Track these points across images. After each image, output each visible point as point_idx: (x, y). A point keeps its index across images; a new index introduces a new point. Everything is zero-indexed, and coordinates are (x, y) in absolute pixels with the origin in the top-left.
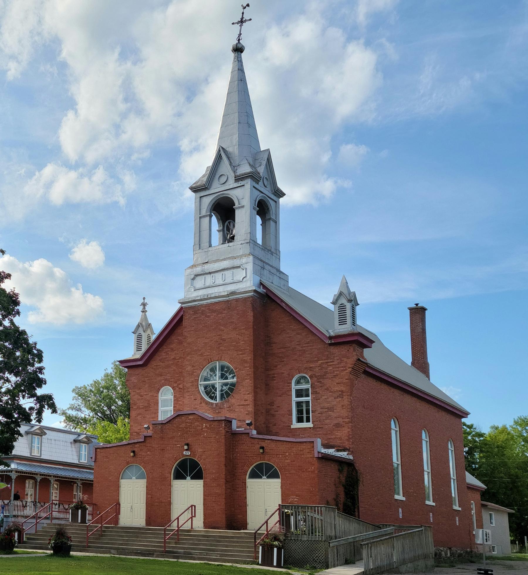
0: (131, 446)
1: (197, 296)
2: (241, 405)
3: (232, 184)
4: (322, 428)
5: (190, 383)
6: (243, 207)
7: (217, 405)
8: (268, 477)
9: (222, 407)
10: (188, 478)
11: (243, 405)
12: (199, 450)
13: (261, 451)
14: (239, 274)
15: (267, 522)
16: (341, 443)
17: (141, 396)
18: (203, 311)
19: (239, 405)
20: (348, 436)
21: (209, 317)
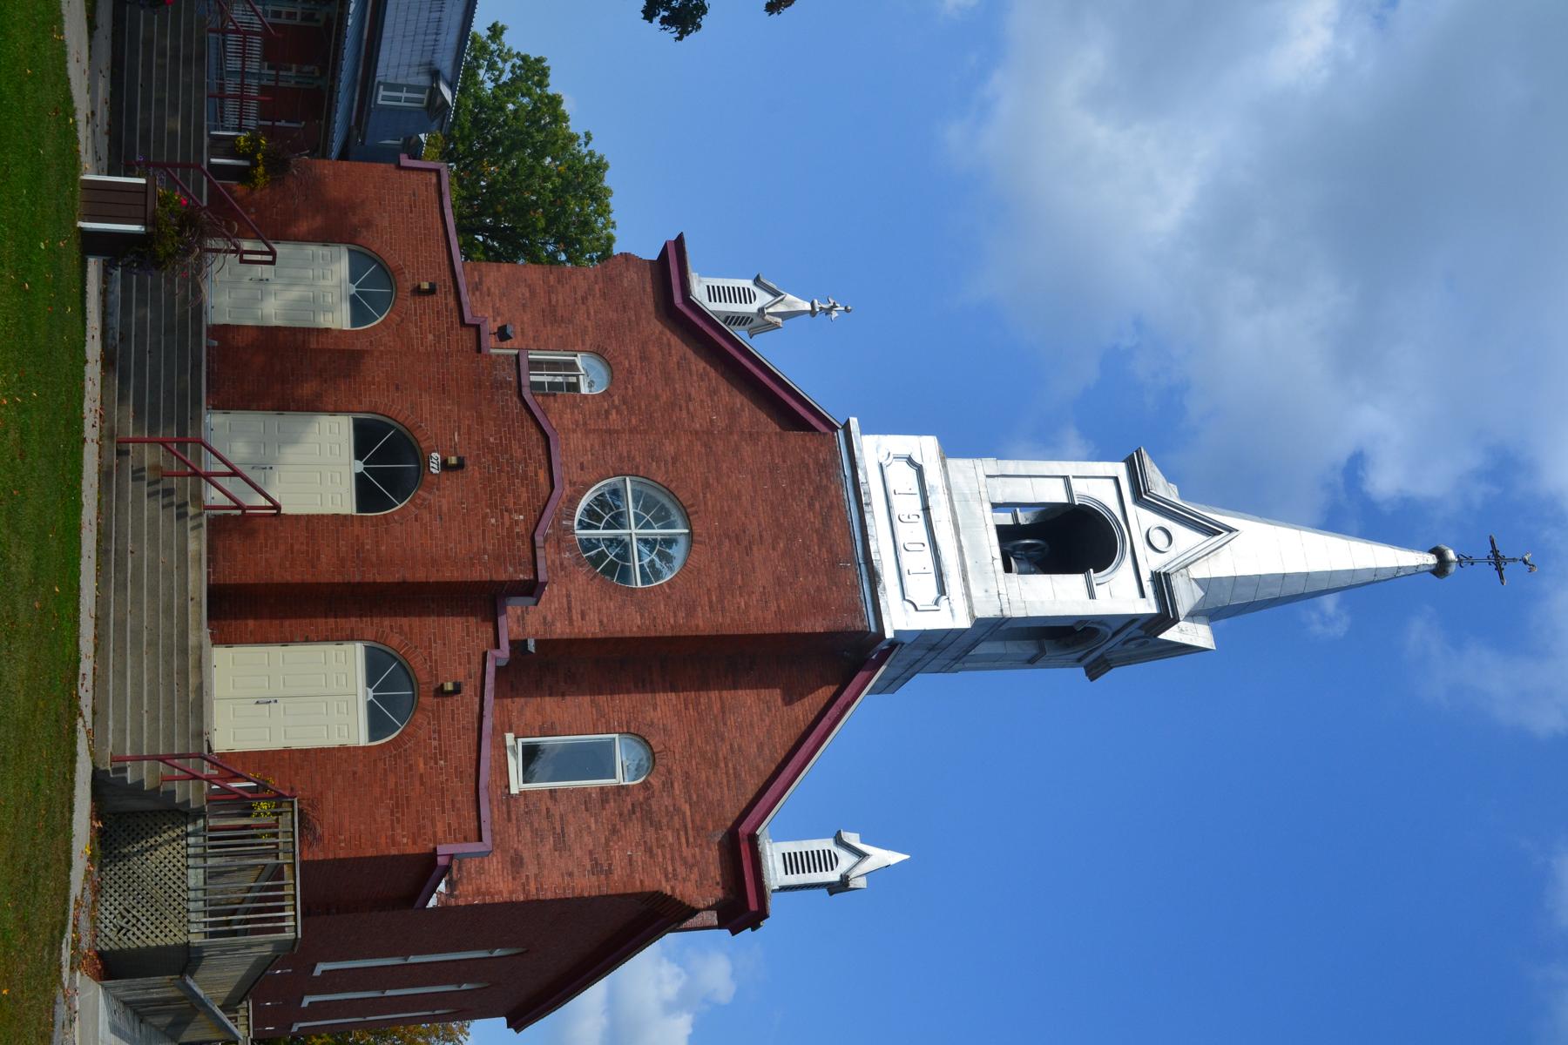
0: (449, 283)
1: (866, 474)
2: (569, 602)
3: (1151, 563)
4: (509, 820)
5: (629, 452)
6: (1092, 595)
7: (570, 530)
8: (370, 704)
9: (563, 545)
10: (359, 466)
11: (570, 609)
12: (444, 501)
13: (449, 687)
14: (922, 588)
15: (235, 473)
16: (469, 873)
17: (584, 299)
18: (827, 489)
19: (568, 596)
20: (489, 893)
21: (811, 506)
